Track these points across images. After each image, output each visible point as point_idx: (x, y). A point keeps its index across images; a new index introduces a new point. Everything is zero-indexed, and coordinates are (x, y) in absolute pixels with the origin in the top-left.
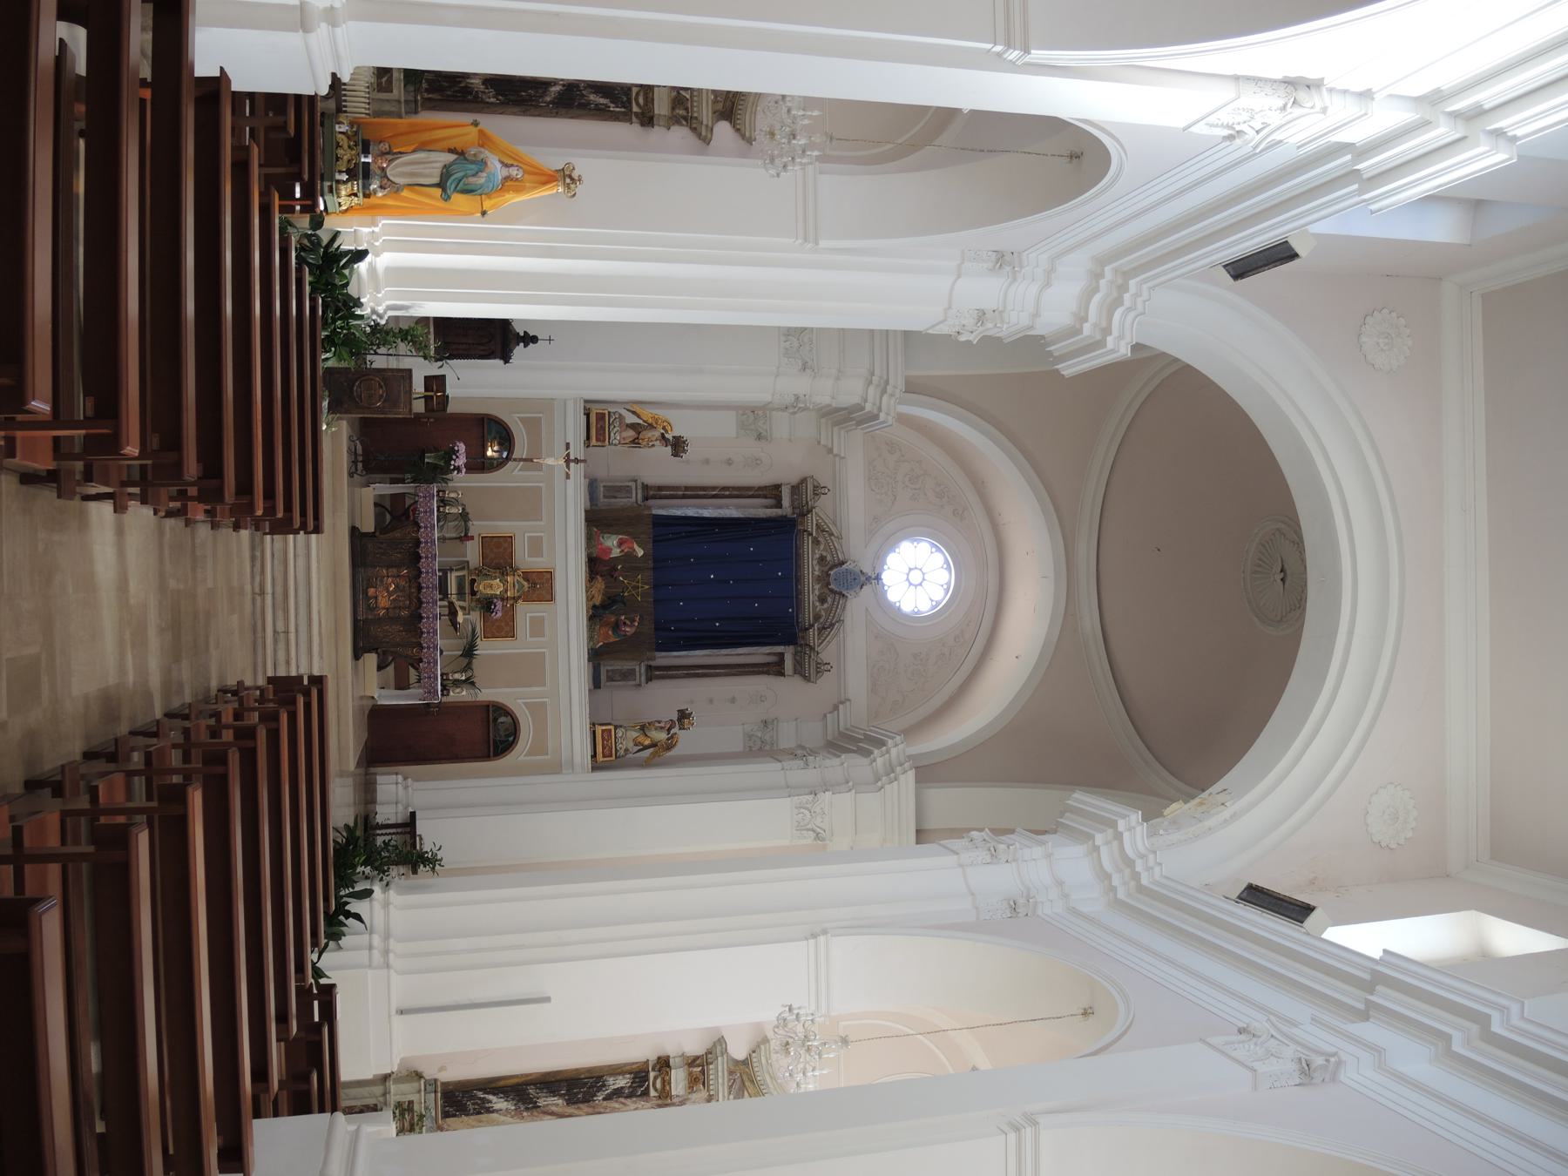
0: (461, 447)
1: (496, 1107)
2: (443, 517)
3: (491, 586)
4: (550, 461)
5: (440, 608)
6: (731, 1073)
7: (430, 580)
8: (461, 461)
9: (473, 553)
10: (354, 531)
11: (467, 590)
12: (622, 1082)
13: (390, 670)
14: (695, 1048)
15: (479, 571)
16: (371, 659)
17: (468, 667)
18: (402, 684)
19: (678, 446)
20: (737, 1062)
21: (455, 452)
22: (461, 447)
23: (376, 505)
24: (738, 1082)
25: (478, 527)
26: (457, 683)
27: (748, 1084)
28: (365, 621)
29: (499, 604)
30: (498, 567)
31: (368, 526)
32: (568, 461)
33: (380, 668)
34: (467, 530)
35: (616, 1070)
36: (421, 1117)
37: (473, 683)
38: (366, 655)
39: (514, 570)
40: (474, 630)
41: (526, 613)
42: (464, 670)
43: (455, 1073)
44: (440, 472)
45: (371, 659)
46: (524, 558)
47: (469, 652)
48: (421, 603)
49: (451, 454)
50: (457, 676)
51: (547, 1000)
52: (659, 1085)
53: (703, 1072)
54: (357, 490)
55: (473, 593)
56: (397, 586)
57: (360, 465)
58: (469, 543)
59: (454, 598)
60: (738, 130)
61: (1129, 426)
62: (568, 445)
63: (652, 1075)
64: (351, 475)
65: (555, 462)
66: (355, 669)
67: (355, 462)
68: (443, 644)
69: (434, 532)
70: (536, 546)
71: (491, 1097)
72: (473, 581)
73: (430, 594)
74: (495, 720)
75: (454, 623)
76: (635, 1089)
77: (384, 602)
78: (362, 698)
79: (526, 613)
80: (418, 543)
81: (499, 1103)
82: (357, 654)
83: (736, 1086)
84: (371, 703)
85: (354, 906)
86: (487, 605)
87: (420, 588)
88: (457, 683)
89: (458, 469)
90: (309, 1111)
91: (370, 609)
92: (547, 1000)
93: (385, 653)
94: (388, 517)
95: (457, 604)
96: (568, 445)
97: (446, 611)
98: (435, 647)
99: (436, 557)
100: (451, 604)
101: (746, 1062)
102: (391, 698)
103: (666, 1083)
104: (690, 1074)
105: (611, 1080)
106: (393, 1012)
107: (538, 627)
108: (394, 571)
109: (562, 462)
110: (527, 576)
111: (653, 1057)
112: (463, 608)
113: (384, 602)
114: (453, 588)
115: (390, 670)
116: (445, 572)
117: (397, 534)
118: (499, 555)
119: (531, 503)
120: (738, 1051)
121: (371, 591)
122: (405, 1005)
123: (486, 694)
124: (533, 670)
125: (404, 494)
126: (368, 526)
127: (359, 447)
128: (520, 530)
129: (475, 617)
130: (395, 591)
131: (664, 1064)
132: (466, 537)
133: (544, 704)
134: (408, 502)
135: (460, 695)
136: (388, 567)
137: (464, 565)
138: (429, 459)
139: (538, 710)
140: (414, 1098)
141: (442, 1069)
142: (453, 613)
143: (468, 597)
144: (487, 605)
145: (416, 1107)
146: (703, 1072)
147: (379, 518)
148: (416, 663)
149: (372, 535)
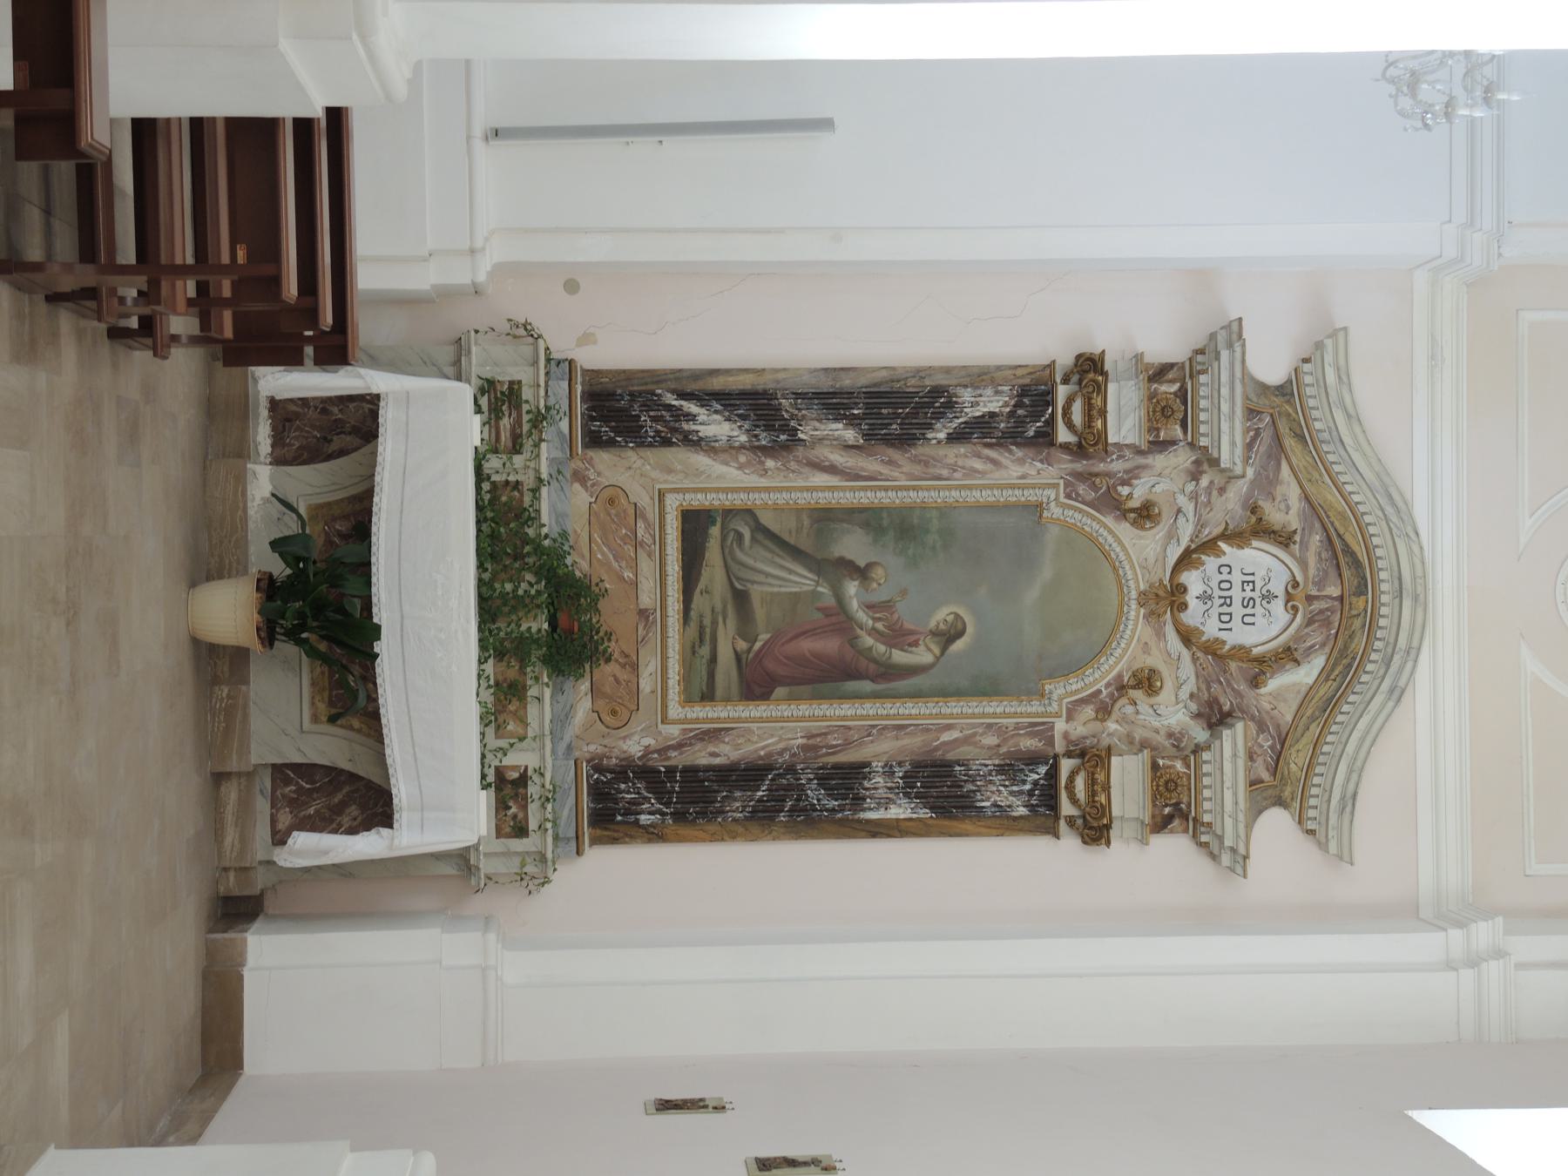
1: (706, 431)
6: (1252, 413)
12: (993, 402)
14: (1165, 341)
19: (1137, 713)
20: (1264, 388)
24: (1266, 436)
27: (1289, 442)
35: (981, 377)
36: (538, 420)
43: (622, 347)
51: (826, 124)
52: (1077, 417)
53: (1182, 395)
63: (1062, 391)
71: (691, 407)
76: (1021, 422)
81: (715, 426)
83: (1262, 446)
90: (233, 123)
92: (826, 124)
101: (1284, 391)
103: (1096, 412)
104: (1152, 396)
105: (966, 396)
106: (478, 131)
111: (1065, 359)
120: (1269, 362)
122: (503, 123)
131: (1090, 368)
140: (523, 374)
141: (586, 339)
145: (527, 394)
146: (1182, 395)
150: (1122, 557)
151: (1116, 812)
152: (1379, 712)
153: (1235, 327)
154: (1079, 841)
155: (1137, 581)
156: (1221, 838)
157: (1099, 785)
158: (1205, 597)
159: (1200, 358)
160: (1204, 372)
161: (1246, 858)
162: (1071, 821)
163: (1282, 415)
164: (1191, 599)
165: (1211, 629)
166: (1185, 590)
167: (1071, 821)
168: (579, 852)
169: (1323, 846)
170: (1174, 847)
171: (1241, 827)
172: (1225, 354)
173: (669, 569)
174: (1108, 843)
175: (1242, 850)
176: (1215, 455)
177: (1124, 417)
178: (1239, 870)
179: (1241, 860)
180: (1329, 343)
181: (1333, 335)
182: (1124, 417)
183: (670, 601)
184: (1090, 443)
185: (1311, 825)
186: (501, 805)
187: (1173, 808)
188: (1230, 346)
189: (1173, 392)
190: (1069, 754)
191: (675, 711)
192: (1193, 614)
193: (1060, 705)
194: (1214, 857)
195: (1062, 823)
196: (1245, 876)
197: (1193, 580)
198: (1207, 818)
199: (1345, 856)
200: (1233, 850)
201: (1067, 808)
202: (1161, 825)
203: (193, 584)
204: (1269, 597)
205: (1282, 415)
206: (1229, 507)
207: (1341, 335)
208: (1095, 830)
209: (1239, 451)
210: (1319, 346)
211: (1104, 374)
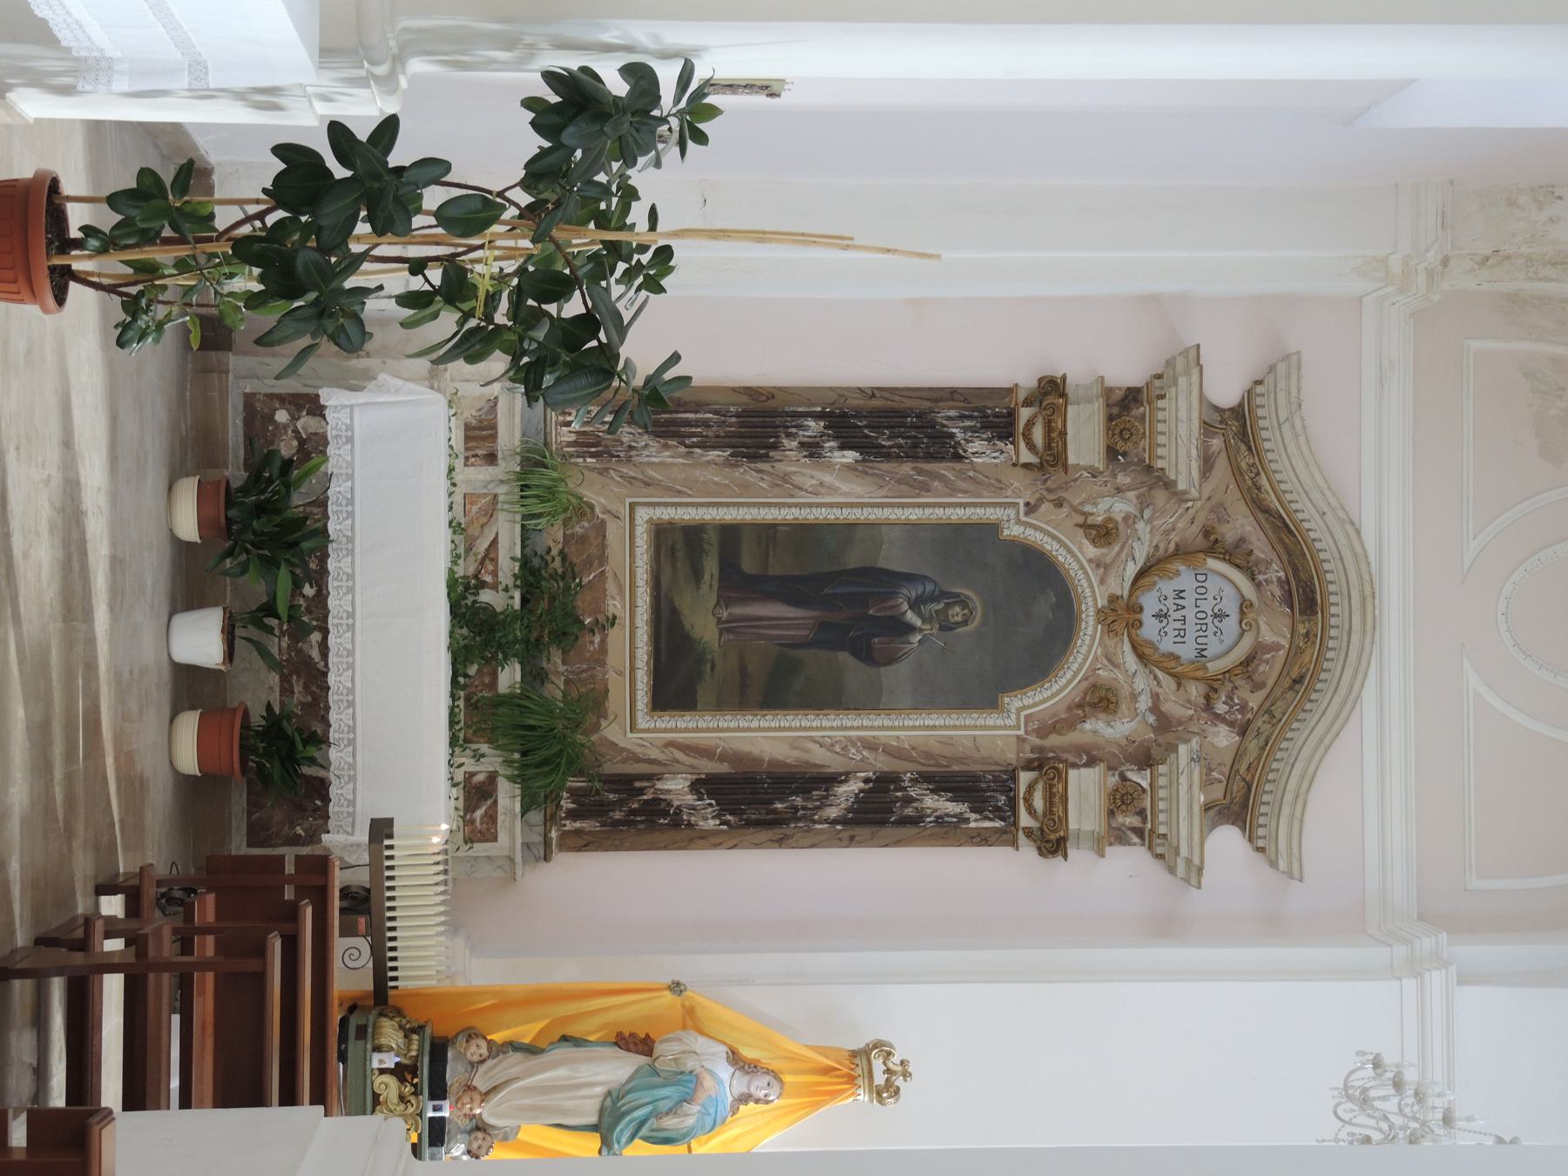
14: (1126, 372)
20: (1216, 409)
63: (1025, 414)
111: (1078, 855)
131: (1051, 390)
150: (1088, 592)
151: (1073, 825)
152: (1332, 724)
153: (1193, 353)
154: (1035, 853)
155: (1095, 600)
156: (1177, 851)
157: (1057, 800)
158: (1161, 616)
159: (1157, 383)
160: (1162, 397)
161: (1200, 870)
162: (1029, 833)
163: (1236, 427)
164: (1147, 617)
165: (1167, 645)
166: (1141, 609)
167: (1029, 833)
168: (547, 858)
169: (1273, 864)
170: (1129, 861)
171: (1196, 837)
172: (1182, 381)
173: (640, 602)
174: (1065, 857)
175: (1196, 861)
176: (1173, 477)
177: (1085, 438)
178: (1194, 881)
179: (1196, 871)
180: (1281, 368)
181: (1287, 358)
182: (1085, 438)
183: (639, 551)
184: (1053, 458)
185: (1260, 843)
186: (470, 807)
187: (1132, 820)
188: (1187, 373)
189: (1126, 408)
190: (1028, 766)
191: (643, 721)
192: (1150, 629)
193: (1018, 719)
194: (1172, 870)
195: (1021, 833)
196: (1199, 887)
197: (1150, 602)
198: (1162, 830)
199: (1294, 874)
200: (1189, 861)
201: (1025, 820)
202: (1119, 837)
203: (173, 612)
204: (1220, 616)
205: (1236, 427)
206: (1181, 525)
207: (1294, 358)
208: (1052, 843)
209: (1195, 474)
210: (1272, 369)
211: (1063, 395)
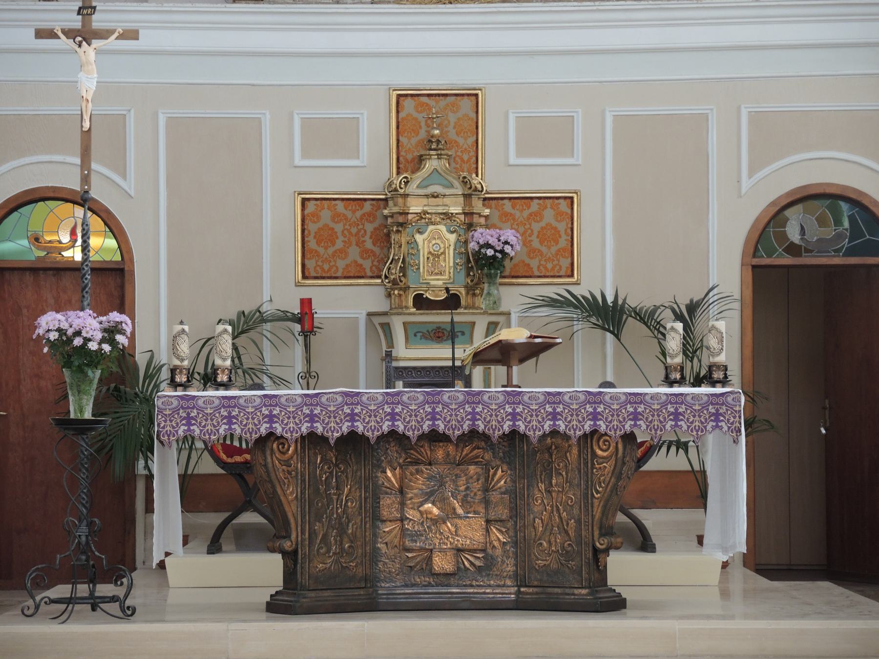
0: (50, 322)
2: (246, 373)
3: (435, 256)
4: (88, 83)
5: (488, 383)
7: (414, 413)
8: (88, 324)
9: (346, 304)
10: (278, 606)
11: (442, 317)
13: (652, 519)
15: (395, 287)
16: (623, 567)
17: (648, 318)
18: (692, 490)
21: (65, 338)
22: (50, 322)
23: (214, 548)
25: (279, 290)
26: (691, 347)
28: (521, 580)
29: (482, 235)
30: (384, 238)
31: (266, 570)
32: (85, 35)
33: (645, 543)
34: (285, 317)
37: (693, 308)
38: (612, 580)
39: (393, 194)
40: (552, 303)
41: (508, 166)
42: (659, 332)
44: (123, 380)
45: (623, 567)
46: (363, 167)
47: (609, 316)
48: (473, 434)
49: (71, 353)
50: (674, 343)
54: (174, 597)
55: (452, 302)
56: (429, 496)
57: (104, 589)
58: (321, 312)
59: (463, 353)
60: (619, 340)
61: (113, 181)
62: (44, 34)
64: (128, 613)
65: (89, 72)
66: (650, 608)
67: (94, 602)
68: (587, 378)
69: (285, 397)
70: (330, 136)
72: (421, 302)
73: (451, 410)
74: (793, 249)
75: (532, 350)
77: (470, 531)
78: (725, 593)
79: (508, 166)
80: (313, 441)
82: (615, 604)
84: (739, 572)
85: (610, 299)
86: (485, 266)
87: (435, 437)
88: (691, 347)
89: (110, 333)
91: (488, 566)
93: (607, 531)
94: (250, 518)
95: (480, 341)
96: (44, 34)
97: (498, 371)
98: (594, 398)
99: (351, 390)
100: (479, 358)
102: (730, 516)
107: (547, 135)
108: (388, 505)
109: (89, 52)
110: (408, 163)
112: (492, 327)
113: (470, 531)
114: (437, 355)
115: (652, 519)
116: (396, 374)
117: (290, 495)
118: (354, 235)
119: (216, 148)
121: (442, 563)
123: (724, 273)
124: (661, 147)
125: (184, 479)
126: (266, 570)
127: (62, 590)
128: (287, 175)
129: (513, 297)
130: (442, 502)
132: (305, 318)
133: (756, 119)
134: (208, 466)
135: (726, 336)
136: (376, 518)
137: (379, 325)
138: (83, 407)
139: (771, 135)
142: (503, 354)
143: (461, 317)
144: (485, 266)
147: (247, 541)
148: (634, 449)
149: (291, 557)
